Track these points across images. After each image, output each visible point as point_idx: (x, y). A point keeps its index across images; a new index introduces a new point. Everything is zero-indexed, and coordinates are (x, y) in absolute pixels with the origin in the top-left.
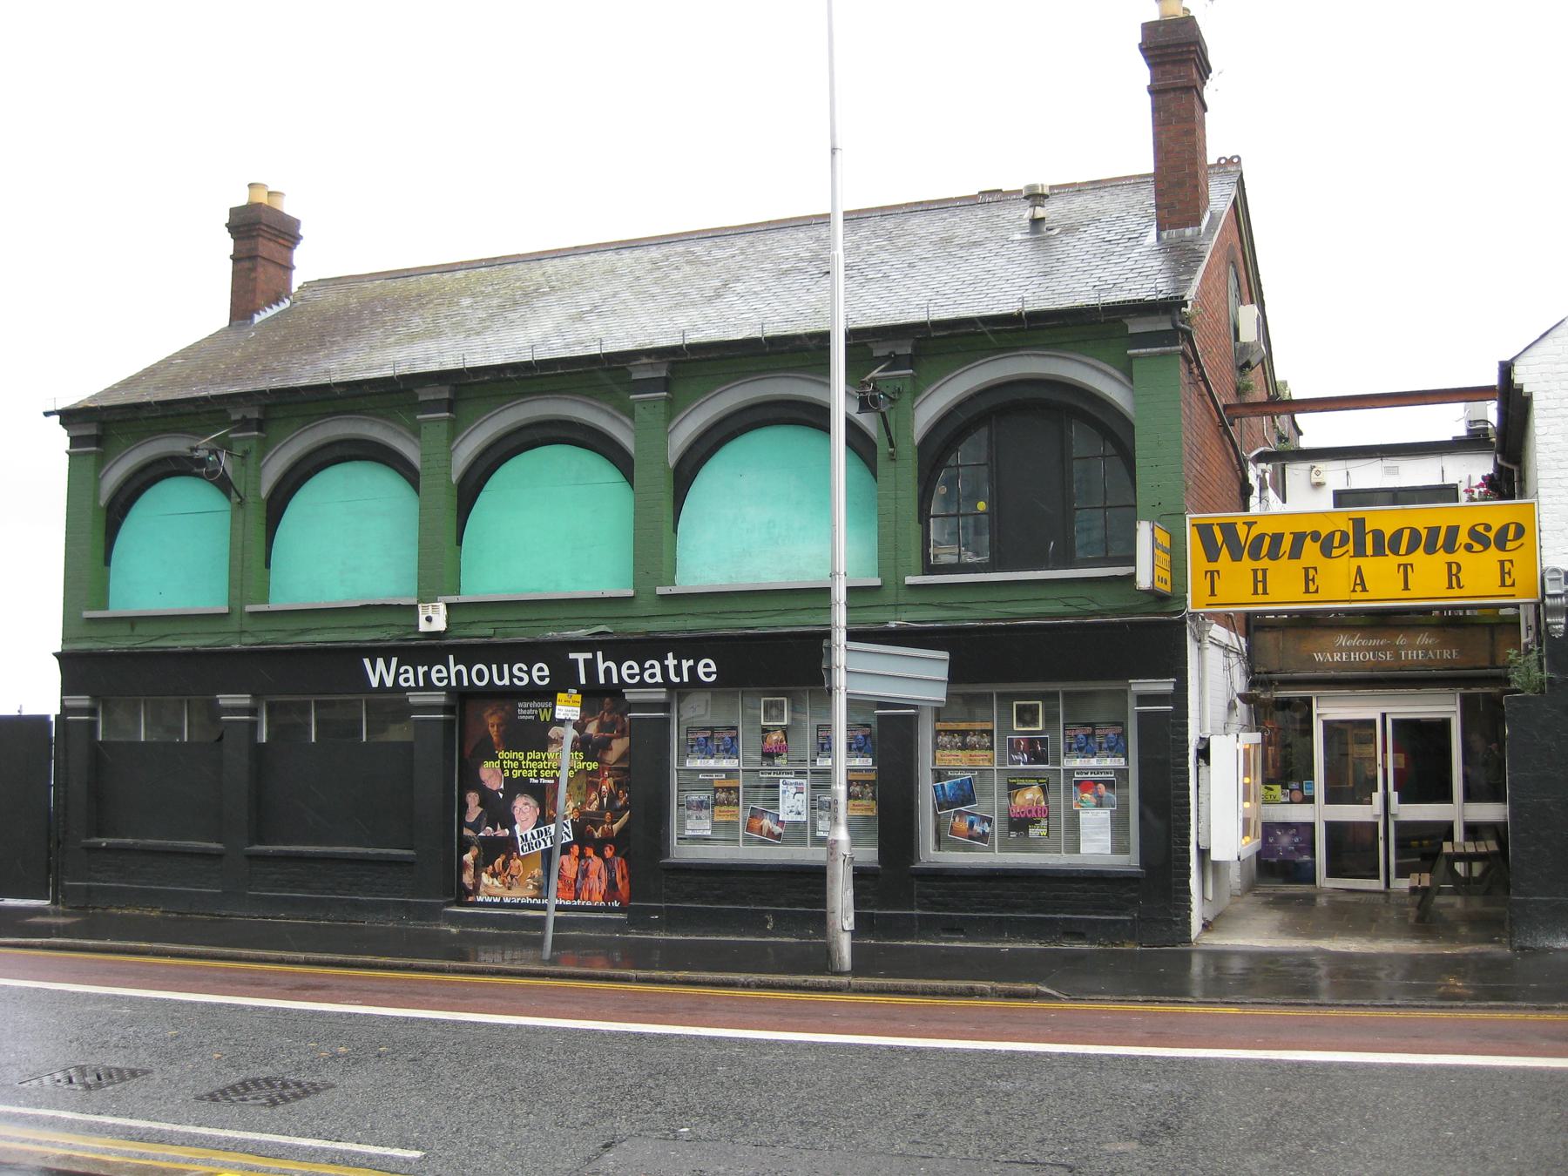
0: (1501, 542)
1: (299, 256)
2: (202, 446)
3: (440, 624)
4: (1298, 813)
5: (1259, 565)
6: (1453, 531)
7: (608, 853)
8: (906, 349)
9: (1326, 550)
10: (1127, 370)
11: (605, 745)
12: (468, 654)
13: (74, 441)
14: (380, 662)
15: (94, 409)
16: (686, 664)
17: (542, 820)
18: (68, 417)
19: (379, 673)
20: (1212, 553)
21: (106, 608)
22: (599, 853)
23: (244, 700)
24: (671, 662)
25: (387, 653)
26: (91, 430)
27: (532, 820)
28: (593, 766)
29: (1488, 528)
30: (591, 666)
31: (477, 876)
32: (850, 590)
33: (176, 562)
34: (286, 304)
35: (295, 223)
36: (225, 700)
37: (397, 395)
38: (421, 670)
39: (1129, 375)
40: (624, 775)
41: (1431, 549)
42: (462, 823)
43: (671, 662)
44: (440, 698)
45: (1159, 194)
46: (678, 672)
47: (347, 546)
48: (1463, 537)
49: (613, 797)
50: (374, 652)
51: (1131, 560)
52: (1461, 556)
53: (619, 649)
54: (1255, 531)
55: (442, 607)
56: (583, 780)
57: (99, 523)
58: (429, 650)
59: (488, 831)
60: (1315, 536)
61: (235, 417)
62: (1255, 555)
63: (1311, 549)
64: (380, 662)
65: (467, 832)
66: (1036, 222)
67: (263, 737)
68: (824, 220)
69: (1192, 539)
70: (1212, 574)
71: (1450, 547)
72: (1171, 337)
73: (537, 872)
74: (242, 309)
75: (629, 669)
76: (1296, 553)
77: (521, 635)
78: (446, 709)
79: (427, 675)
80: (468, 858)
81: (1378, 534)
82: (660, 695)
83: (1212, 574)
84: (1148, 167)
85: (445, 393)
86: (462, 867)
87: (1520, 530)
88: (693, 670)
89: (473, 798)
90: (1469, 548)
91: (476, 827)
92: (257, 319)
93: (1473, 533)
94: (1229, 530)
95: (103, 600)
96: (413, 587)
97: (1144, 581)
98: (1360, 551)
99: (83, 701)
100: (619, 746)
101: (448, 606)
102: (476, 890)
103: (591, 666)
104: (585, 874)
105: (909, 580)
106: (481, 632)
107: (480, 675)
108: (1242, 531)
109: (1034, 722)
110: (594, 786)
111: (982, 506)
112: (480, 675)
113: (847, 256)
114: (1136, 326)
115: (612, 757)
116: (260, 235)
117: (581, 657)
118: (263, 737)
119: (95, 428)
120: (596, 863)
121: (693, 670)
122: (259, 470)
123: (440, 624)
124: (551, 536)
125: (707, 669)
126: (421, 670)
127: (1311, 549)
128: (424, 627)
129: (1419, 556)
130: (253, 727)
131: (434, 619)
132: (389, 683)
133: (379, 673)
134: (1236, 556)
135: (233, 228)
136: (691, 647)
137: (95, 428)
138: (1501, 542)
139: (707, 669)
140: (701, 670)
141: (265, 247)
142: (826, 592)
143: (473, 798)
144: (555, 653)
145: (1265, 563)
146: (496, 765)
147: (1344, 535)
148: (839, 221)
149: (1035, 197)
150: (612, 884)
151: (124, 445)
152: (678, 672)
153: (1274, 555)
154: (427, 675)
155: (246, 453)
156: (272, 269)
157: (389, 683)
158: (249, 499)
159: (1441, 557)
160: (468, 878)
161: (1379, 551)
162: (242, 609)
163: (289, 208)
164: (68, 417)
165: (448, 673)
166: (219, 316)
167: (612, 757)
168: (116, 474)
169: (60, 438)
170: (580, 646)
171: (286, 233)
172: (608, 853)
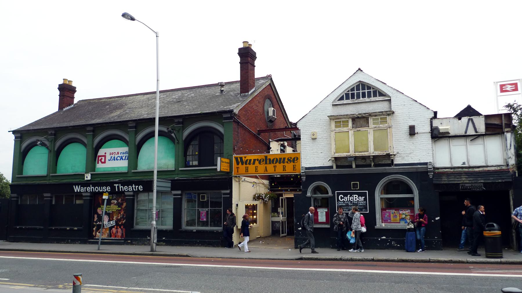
0: (294, 161)
1: (76, 95)
2: (78, 136)
3: (89, 178)
4: (276, 219)
5: (247, 166)
6: (284, 159)
7: (122, 227)
8: (181, 120)
9: (260, 163)
10: (223, 125)
11: (122, 204)
12: (94, 185)
13: (16, 138)
14: (77, 186)
15: (21, 131)
16: (137, 187)
17: (109, 221)
18: (14, 132)
19: (77, 189)
20: (238, 164)
21: (56, 173)
22: (120, 228)
23: (49, 195)
24: (134, 186)
25: (78, 184)
26: (19, 135)
27: (107, 221)
28: (120, 208)
29: (291, 158)
30: (118, 187)
31: (96, 233)
32: (158, 171)
33: (37, 165)
34: (73, 106)
35: (75, 88)
36: (45, 195)
37: (122, 125)
38: (137, 187)
39: (223, 125)
40: (126, 210)
41: (280, 163)
42: (93, 221)
43: (134, 186)
44: (89, 194)
45: (241, 85)
46: (135, 189)
47: (73, 160)
48: (286, 160)
49: (123, 215)
50: (76, 184)
51: (216, 165)
52: (286, 164)
53: (124, 184)
54: (246, 159)
55: (90, 175)
56: (118, 212)
57: (21, 156)
58: (86, 184)
59: (98, 223)
60: (258, 160)
61: (50, 133)
62: (246, 164)
63: (257, 162)
64: (77, 186)
65: (95, 223)
66: (222, 91)
67: (54, 203)
68: (155, 93)
69: (234, 160)
70: (238, 168)
71: (284, 162)
72: (231, 118)
73: (108, 232)
74: (61, 107)
75: (126, 188)
76: (254, 163)
77: (105, 180)
78: (90, 196)
79: (86, 189)
80: (94, 229)
81: (270, 159)
82: (132, 193)
83: (238, 168)
84: (239, 79)
85: (92, 129)
86: (93, 231)
87: (297, 159)
88: (138, 188)
89: (96, 216)
90: (287, 162)
91: (96, 222)
92: (64, 109)
93: (288, 159)
94: (241, 158)
95: (136, 167)
96: (85, 170)
97: (219, 170)
98: (266, 163)
99: (15, 195)
100: (125, 204)
101: (91, 174)
102: (96, 236)
103: (118, 187)
104: (117, 232)
105: (180, 169)
106: (98, 180)
107: (97, 189)
108: (244, 159)
109: (204, 199)
110: (120, 213)
111: (197, 153)
112: (97, 189)
113: (155, 103)
114: (225, 116)
115: (124, 206)
116: (66, 91)
117: (116, 185)
118: (54, 203)
119: (21, 135)
120: (119, 230)
121: (138, 188)
122: (183, 133)
123: (89, 178)
124: (114, 159)
125: (141, 188)
126: (85, 188)
127: (257, 162)
128: (86, 179)
129: (277, 164)
130: (51, 201)
131: (88, 177)
132: (79, 191)
133: (77, 189)
134: (242, 164)
135: (59, 89)
136: (137, 183)
137: (21, 135)
138: (294, 161)
139: (141, 188)
140: (139, 188)
141: (67, 94)
142: (153, 172)
143: (96, 216)
144: (111, 184)
145: (248, 165)
146: (100, 208)
147: (263, 159)
148: (158, 92)
149: (221, 85)
150: (122, 234)
151: (26, 139)
152: (135, 189)
153: (250, 164)
154: (86, 189)
155: (180, 129)
156: (68, 98)
157: (79, 191)
158: (52, 151)
159: (282, 164)
160: (94, 234)
161: (270, 163)
162: (178, 169)
163: (73, 85)
164: (14, 132)
165: (90, 189)
166: (55, 109)
167: (124, 206)
168: (24, 145)
169: (13, 137)
170: (116, 183)
171: (73, 90)
172: (122, 227)
